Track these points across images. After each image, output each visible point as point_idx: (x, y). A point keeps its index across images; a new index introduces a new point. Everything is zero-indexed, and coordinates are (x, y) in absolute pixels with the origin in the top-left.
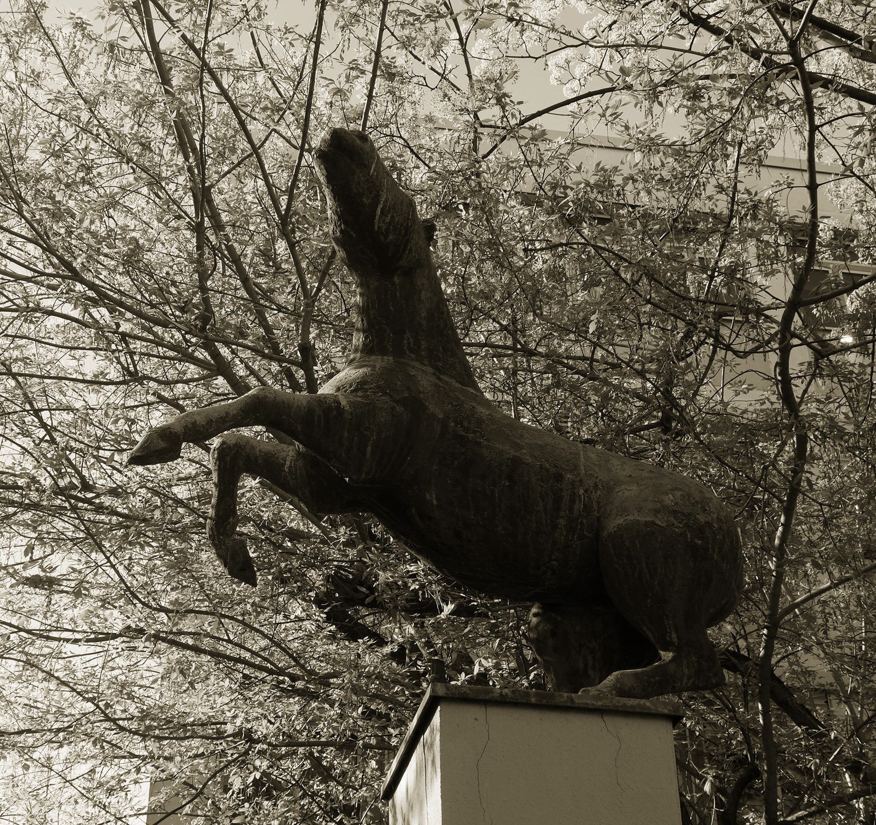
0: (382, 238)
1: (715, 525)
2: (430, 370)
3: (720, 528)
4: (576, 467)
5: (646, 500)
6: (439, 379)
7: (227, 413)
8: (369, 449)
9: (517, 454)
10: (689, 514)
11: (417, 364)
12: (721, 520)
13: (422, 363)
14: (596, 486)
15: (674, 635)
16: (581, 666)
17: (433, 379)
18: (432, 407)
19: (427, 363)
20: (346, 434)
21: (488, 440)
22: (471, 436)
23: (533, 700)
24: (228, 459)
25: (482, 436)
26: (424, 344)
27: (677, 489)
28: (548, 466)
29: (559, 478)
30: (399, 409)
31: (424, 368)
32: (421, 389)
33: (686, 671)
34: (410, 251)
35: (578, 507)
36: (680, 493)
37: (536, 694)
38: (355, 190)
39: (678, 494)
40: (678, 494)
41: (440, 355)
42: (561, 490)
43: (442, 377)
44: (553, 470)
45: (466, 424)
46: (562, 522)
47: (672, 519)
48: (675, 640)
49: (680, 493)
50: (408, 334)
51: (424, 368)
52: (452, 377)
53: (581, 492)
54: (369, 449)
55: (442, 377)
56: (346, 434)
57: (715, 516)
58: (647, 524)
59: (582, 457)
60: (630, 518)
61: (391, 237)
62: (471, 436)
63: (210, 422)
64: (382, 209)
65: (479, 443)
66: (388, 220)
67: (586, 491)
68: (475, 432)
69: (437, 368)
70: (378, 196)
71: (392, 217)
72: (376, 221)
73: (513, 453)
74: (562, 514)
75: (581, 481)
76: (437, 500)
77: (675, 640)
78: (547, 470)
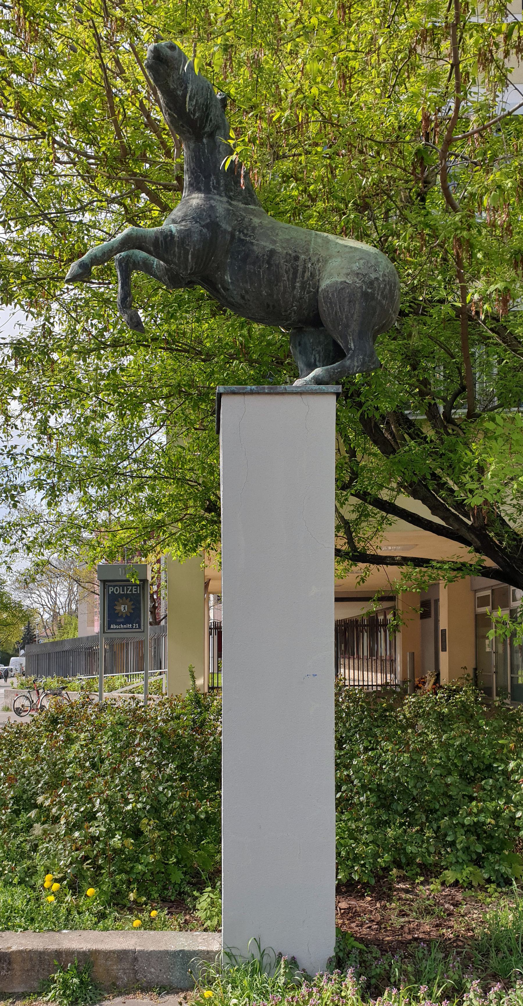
0: (192, 116)
1: (381, 279)
2: (225, 199)
3: (384, 280)
4: (308, 250)
5: (343, 268)
6: (230, 204)
7: (113, 247)
8: (190, 256)
9: (273, 247)
10: (366, 274)
11: (217, 197)
12: (385, 275)
13: (221, 196)
14: (318, 261)
15: (352, 345)
16: (313, 360)
17: (226, 206)
18: (225, 226)
19: (223, 194)
20: (176, 250)
21: (257, 240)
22: (248, 239)
23: (266, 391)
24: (123, 264)
25: (254, 238)
26: (222, 182)
27: (361, 259)
28: (290, 252)
29: (297, 258)
30: (205, 230)
31: (221, 199)
32: (218, 215)
33: (356, 364)
34: (211, 120)
35: (307, 274)
36: (364, 261)
37: (268, 388)
38: (172, 87)
39: (362, 262)
40: (362, 262)
41: (233, 188)
42: (298, 266)
43: (233, 202)
44: (294, 254)
45: (245, 232)
46: (298, 284)
47: (355, 278)
48: (353, 347)
49: (364, 261)
50: (213, 178)
51: (221, 199)
52: (239, 201)
53: (310, 265)
54: (190, 256)
55: (233, 202)
56: (176, 250)
57: (381, 273)
58: (342, 283)
59: (313, 242)
60: (333, 280)
61: (197, 115)
62: (248, 239)
63: (104, 254)
64: (190, 97)
65: (252, 243)
66: (194, 103)
67: (312, 264)
68: (250, 236)
69: (230, 198)
70: (186, 88)
71: (197, 100)
72: (187, 105)
73: (271, 247)
74: (298, 280)
75: (310, 259)
76: (231, 279)
77: (353, 347)
78: (290, 255)
